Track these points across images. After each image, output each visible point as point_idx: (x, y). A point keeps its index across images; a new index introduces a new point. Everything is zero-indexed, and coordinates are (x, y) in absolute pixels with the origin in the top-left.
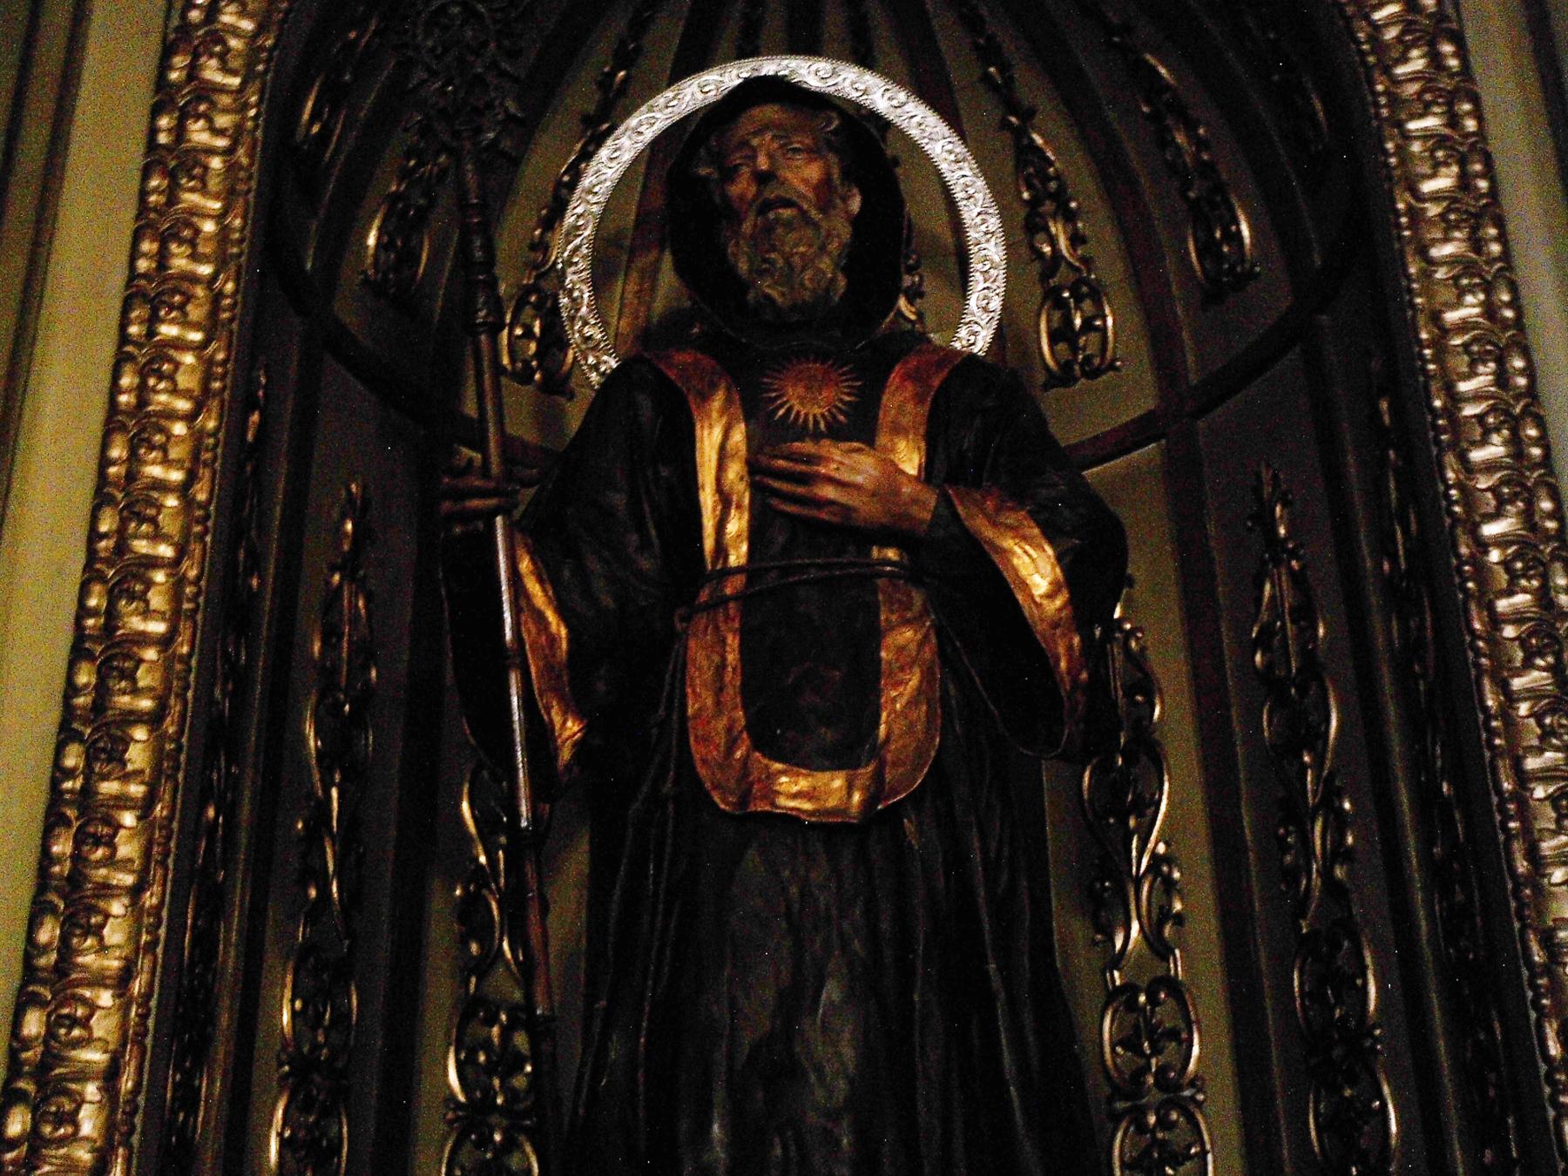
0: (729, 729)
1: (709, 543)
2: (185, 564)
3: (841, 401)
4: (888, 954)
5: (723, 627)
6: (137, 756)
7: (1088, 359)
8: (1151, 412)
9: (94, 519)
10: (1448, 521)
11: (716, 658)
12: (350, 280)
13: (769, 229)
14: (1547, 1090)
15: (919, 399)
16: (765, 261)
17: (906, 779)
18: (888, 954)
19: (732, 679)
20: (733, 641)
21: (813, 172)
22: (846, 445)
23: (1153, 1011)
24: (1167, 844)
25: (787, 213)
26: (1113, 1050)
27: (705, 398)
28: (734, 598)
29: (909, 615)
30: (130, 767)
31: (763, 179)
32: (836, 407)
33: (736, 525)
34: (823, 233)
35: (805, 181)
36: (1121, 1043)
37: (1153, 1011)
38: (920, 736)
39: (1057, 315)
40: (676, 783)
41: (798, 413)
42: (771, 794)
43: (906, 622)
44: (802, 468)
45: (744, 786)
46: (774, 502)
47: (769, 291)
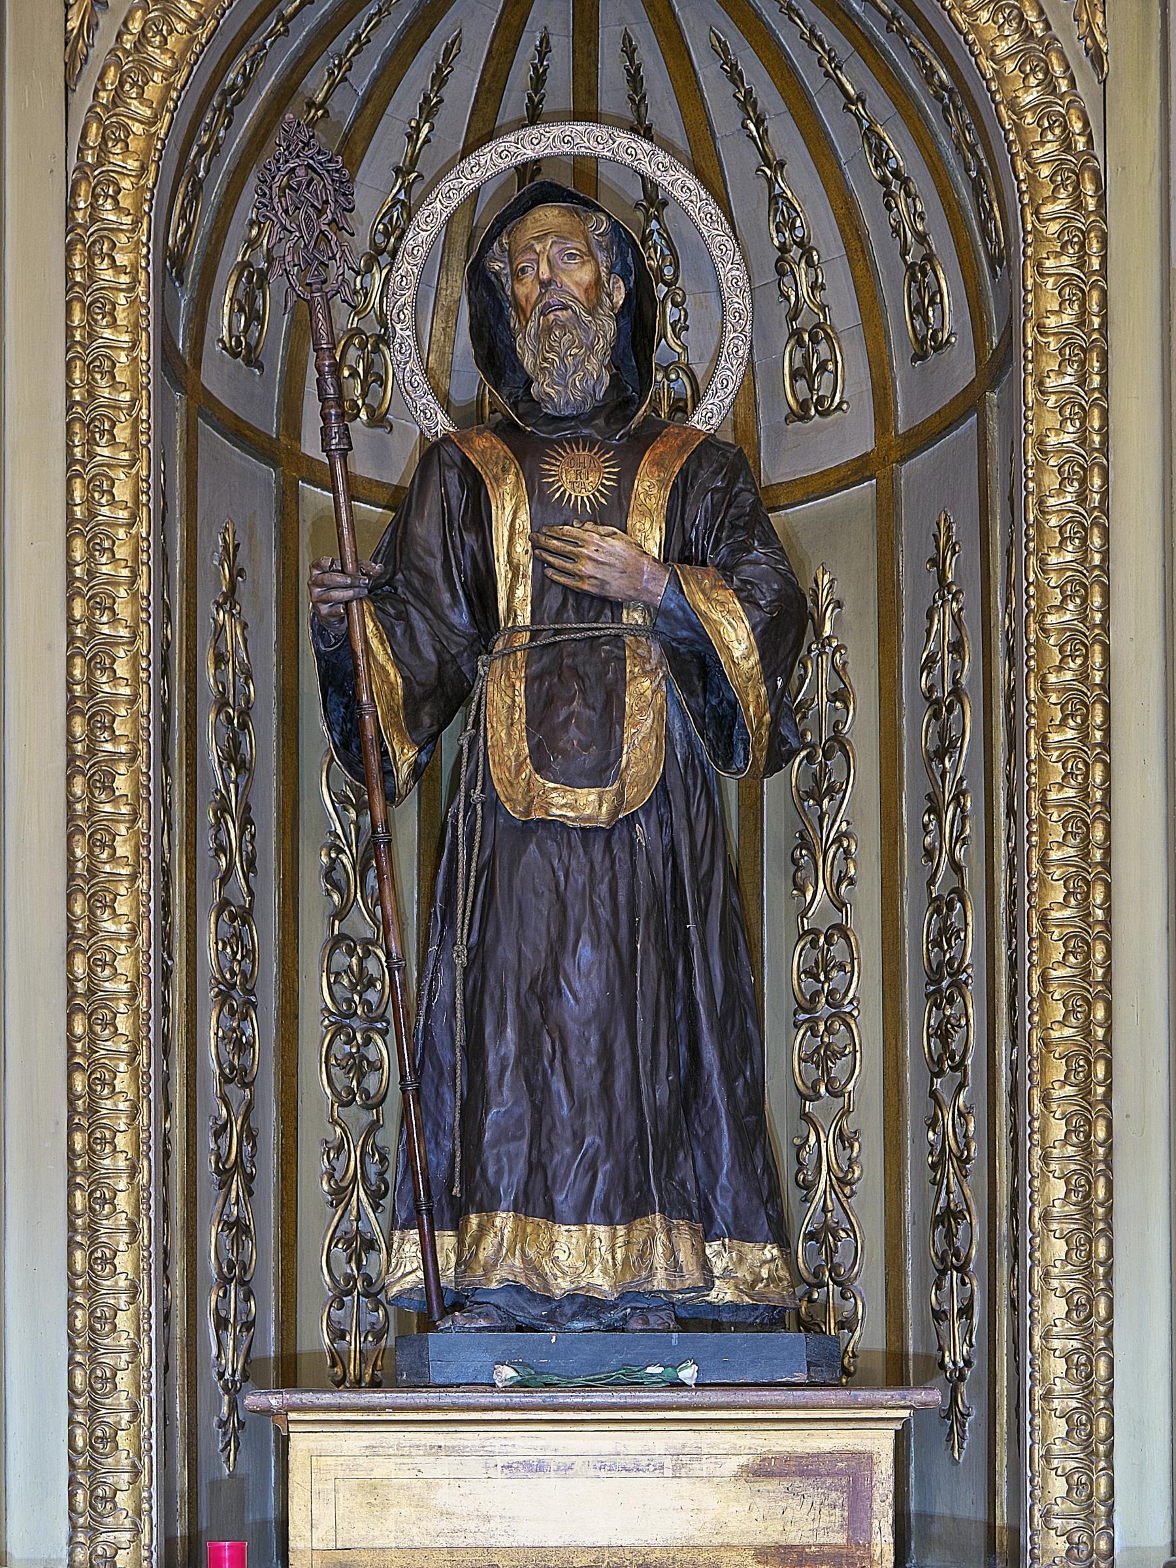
0: (518, 756)
1: (502, 605)
2: (138, 642)
3: (603, 485)
4: (623, 917)
5: (513, 675)
6: (122, 785)
7: (821, 400)
8: (867, 454)
9: (70, 609)
10: (1026, 610)
11: (508, 701)
12: (212, 349)
13: (549, 330)
14: (1028, 1012)
15: (662, 483)
16: (545, 360)
17: (638, 795)
18: (623, 917)
19: (520, 716)
20: (520, 686)
21: (585, 275)
22: (603, 529)
23: (828, 950)
24: (848, 823)
25: (563, 315)
26: (799, 977)
27: (498, 480)
28: (522, 648)
29: (648, 667)
30: (117, 793)
31: (545, 285)
32: (599, 491)
33: (524, 591)
34: (592, 333)
35: (577, 284)
36: (805, 972)
37: (828, 950)
38: (651, 763)
39: (799, 354)
40: (482, 792)
41: (570, 495)
42: (547, 806)
43: (645, 673)
44: (569, 548)
45: (528, 799)
46: (549, 572)
47: (548, 390)
